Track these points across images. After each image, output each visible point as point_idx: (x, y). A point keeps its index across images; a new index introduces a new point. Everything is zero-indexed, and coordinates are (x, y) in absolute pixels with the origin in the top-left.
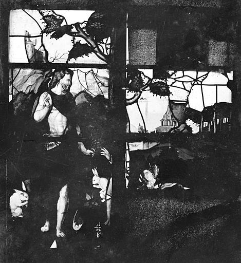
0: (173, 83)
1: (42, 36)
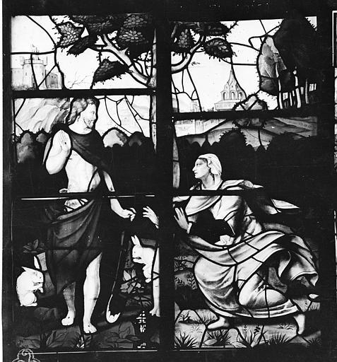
0: (256, 253)
1: (55, 52)
